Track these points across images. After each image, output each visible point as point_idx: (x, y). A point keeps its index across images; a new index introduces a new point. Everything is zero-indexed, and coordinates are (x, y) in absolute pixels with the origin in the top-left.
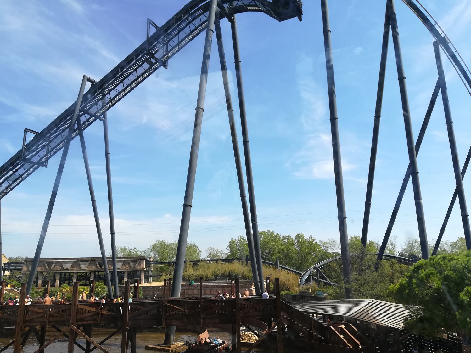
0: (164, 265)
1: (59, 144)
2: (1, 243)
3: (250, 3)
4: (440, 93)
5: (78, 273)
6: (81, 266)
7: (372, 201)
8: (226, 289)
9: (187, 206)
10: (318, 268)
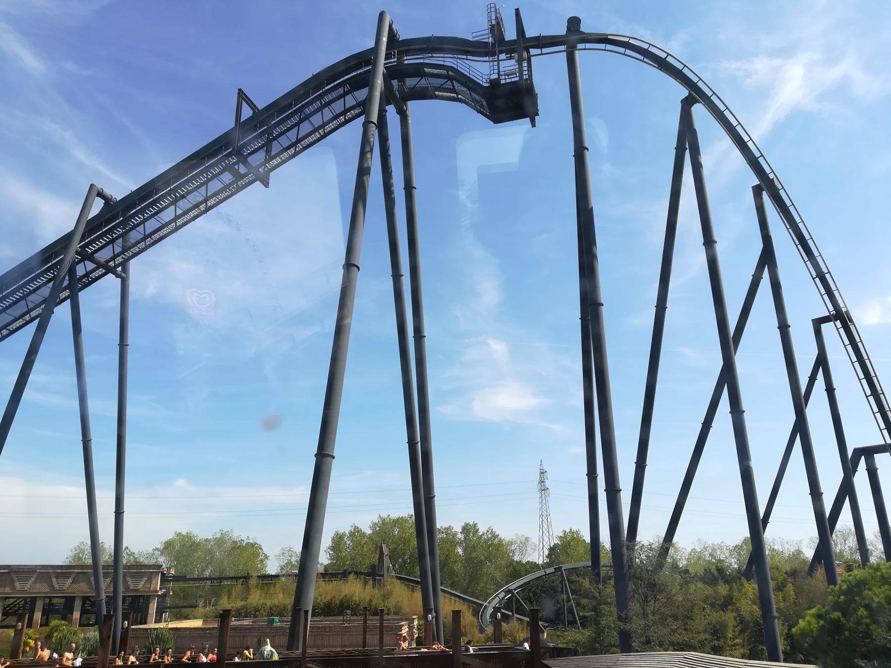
0: (190, 584)
1: (16, 319)
2: (123, 513)
3: (442, 85)
4: (766, 274)
5: (6, 598)
6: (17, 584)
7: (649, 461)
8: (348, 634)
9: (323, 455)
10: (513, 591)
